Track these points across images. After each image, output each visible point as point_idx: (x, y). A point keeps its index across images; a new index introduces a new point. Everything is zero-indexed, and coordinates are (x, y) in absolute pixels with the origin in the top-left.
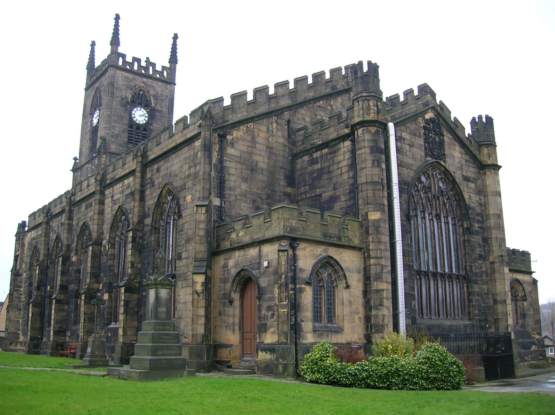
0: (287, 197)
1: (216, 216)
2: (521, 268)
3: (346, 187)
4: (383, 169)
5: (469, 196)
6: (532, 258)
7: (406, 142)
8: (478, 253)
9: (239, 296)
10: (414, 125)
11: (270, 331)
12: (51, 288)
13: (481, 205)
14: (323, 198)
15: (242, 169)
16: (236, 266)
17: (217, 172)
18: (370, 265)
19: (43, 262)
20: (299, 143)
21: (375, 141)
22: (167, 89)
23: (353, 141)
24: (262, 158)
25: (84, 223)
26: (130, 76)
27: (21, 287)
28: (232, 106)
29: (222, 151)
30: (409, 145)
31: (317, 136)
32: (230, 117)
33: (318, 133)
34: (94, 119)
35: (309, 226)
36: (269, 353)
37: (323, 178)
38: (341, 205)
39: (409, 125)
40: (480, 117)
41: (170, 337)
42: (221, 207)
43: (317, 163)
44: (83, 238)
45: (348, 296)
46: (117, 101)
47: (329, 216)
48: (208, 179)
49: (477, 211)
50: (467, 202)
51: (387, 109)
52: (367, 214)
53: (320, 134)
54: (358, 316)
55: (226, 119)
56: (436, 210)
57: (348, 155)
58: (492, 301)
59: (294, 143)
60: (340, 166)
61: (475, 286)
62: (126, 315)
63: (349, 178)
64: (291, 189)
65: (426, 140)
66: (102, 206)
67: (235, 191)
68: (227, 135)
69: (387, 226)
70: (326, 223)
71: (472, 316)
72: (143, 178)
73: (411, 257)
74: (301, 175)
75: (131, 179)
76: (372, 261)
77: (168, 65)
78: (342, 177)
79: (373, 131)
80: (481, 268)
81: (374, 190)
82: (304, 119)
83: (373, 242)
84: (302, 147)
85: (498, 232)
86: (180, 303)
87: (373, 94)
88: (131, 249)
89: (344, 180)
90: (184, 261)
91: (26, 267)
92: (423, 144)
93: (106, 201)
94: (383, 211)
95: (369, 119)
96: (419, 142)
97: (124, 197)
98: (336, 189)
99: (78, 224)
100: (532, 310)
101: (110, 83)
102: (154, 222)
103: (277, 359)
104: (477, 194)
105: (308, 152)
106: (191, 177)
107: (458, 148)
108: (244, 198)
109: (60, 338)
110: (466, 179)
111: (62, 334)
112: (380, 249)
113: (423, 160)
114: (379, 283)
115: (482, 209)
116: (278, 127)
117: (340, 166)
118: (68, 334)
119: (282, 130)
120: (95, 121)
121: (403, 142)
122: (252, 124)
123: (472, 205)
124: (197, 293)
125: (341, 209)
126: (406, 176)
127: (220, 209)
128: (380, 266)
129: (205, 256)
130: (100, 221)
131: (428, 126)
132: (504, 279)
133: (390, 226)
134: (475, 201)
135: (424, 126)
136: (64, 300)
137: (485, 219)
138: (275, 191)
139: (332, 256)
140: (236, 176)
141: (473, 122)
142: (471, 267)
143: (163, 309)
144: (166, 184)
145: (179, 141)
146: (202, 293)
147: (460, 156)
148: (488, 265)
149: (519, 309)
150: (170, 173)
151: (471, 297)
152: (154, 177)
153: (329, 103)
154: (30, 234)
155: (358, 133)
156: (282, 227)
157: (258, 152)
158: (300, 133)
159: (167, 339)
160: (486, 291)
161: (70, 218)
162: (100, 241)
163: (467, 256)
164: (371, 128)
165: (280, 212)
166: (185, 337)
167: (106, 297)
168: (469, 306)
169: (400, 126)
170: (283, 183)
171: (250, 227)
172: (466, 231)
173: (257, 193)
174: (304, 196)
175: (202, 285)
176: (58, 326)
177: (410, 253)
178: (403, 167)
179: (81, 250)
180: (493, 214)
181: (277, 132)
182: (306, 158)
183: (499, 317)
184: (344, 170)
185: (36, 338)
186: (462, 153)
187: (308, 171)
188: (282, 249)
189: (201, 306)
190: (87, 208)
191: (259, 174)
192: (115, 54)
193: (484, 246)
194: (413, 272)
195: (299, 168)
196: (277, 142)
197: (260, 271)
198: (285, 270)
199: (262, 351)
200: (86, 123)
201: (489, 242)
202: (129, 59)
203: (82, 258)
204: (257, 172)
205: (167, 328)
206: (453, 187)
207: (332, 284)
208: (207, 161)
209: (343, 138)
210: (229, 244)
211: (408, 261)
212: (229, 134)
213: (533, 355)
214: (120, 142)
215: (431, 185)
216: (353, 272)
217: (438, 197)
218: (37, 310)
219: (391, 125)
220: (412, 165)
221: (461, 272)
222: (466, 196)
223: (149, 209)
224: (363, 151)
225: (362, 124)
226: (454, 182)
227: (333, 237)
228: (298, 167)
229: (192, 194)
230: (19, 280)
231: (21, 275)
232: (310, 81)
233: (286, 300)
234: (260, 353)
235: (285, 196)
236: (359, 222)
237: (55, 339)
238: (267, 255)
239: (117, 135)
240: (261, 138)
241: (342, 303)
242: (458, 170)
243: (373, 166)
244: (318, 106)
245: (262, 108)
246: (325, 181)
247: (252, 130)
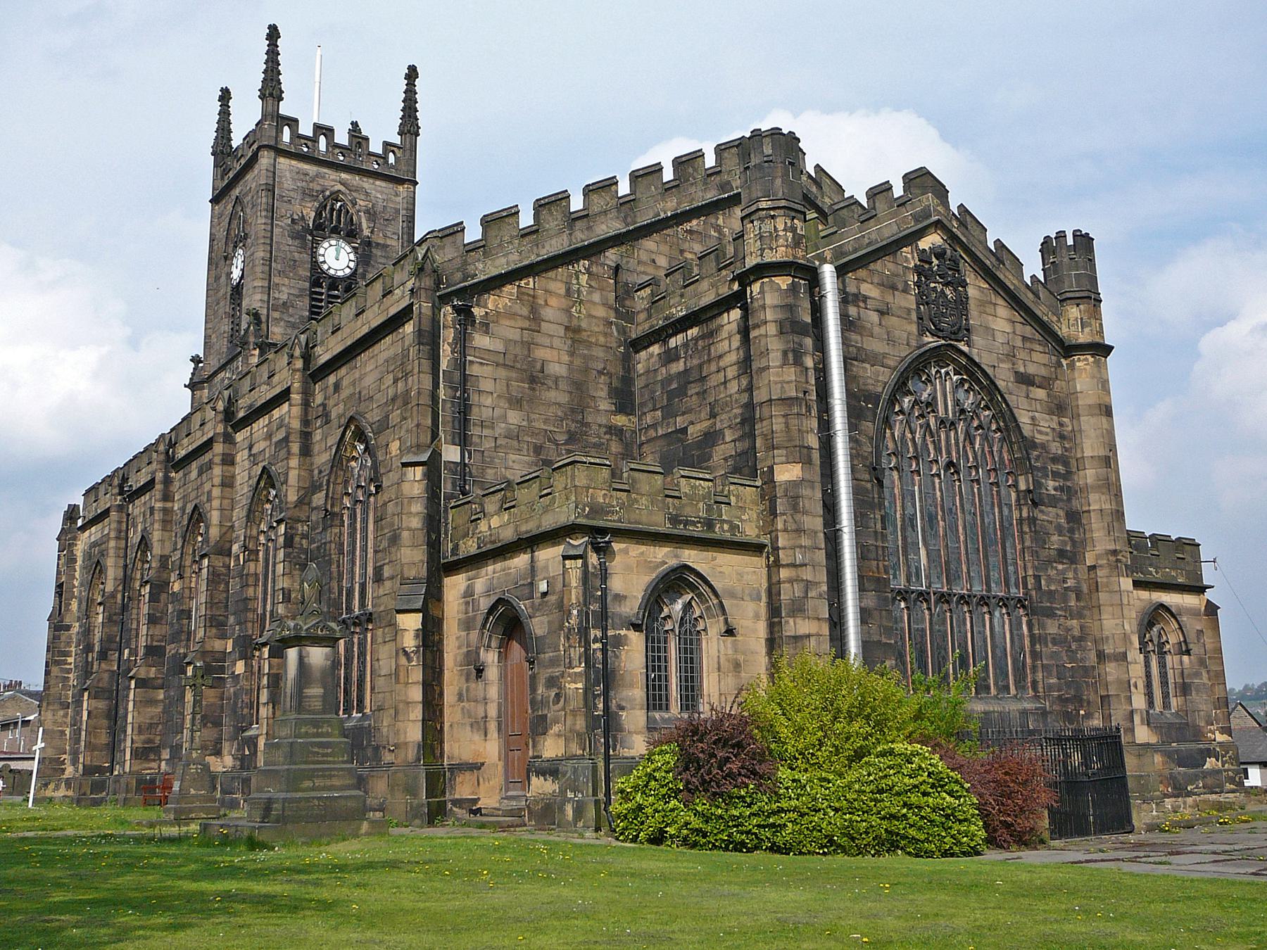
0: (616, 435)
1: (449, 486)
2: (1176, 578)
3: (735, 411)
5: (1033, 418)
6: (1204, 554)
7: (870, 303)
8: (1056, 546)
9: (496, 657)
10: (890, 266)
11: (552, 732)
12: (130, 654)
13: (1062, 437)
14: (689, 437)
15: (508, 380)
16: (488, 593)
17: (451, 388)
18: (779, 582)
19: (113, 595)
20: (642, 316)
21: (790, 308)
22: (397, 195)
23: (745, 309)
24: (555, 353)
25: (196, 506)
26: (311, 169)
27: (68, 654)
28: (483, 243)
29: (462, 342)
30: (878, 311)
31: (678, 299)
32: (480, 266)
33: (679, 292)
34: (234, 268)
35: (636, 501)
36: (550, 779)
37: (689, 393)
38: (723, 451)
39: (877, 266)
41: (330, 750)
42: (463, 464)
43: (677, 358)
44: (195, 539)
45: (730, 652)
46: (281, 227)
47: (683, 477)
48: (429, 406)
49: (1054, 450)
50: (1027, 430)
51: (822, 234)
52: (771, 469)
53: (682, 296)
55: (471, 269)
56: (949, 453)
57: (736, 341)
58: (1093, 656)
59: (629, 316)
60: (722, 364)
61: (1049, 622)
62: (273, 708)
63: (740, 392)
64: (624, 418)
65: (922, 299)
66: (231, 468)
67: (493, 428)
68: (472, 307)
69: (818, 495)
70: (676, 494)
71: (1041, 690)
72: (306, 404)
73: (884, 560)
74: (647, 386)
75: (286, 406)
76: (784, 573)
77: (397, 140)
78: (726, 388)
79: (784, 287)
80: (1064, 581)
81: (785, 416)
82: (654, 261)
83: (785, 530)
84: (647, 326)
86: (379, 676)
87: (783, 203)
88: (284, 561)
89: (730, 396)
90: (388, 584)
91: (79, 608)
92: (914, 307)
93: (238, 458)
94: (807, 461)
95: (774, 259)
96: (904, 304)
97: (273, 447)
98: (715, 417)
99: (183, 509)
100: (1205, 675)
101: (264, 187)
102: (329, 502)
103: (563, 792)
104: (1051, 413)
105: (658, 336)
106: (399, 402)
107: (1003, 311)
108: (515, 443)
109: (147, 766)
110: (1025, 380)
111: (152, 757)
112: (801, 547)
113: (914, 343)
114: (799, 621)
115: (1067, 446)
116: (593, 284)
117: (722, 364)
118: (166, 754)
119: (602, 290)
120: (236, 274)
121: (862, 304)
122: (531, 280)
123: (1040, 438)
124: (406, 653)
125: (725, 459)
126: (870, 381)
127: (461, 468)
128: (802, 585)
129: (424, 573)
130: (226, 502)
131: (927, 266)
132: (1122, 605)
133: (824, 492)
134: (1048, 430)
135: (915, 265)
136: (156, 678)
137: (1074, 470)
138: (588, 425)
139: (691, 564)
140: (495, 395)
141: (1048, 248)
142: (1037, 578)
143: (315, 691)
144: (351, 419)
145: (375, 324)
146: (416, 652)
147: (1008, 329)
148: (1083, 574)
149: (1170, 673)
150: (360, 392)
151: (1038, 646)
152: (331, 402)
153: (713, 221)
154: (87, 533)
155: (751, 292)
156: (572, 506)
157: (547, 341)
158: (643, 293)
159: (324, 755)
160: (1076, 633)
161: (167, 497)
162: (228, 545)
164: (777, 280)
165: (569, 473)
166: (390, 750)
167: (240, 667)
168: (1034, 668)
169: (855, 270)
170: (605, 405)
171: (513, 507)
172: (1025, 498)
173: (546, 430)
174: (652, 433)
175: (417, 636)
176: (142, 737)
177: (880, 552)
178: (863, 362)
179: (191, 566)
181: (589, 293)
182: (655, 349)
184: (732, 372)
185: (100, 770)
187: (659, 378)
188: (572, 553)
189: (415, 680)
190: (200, 474)
191: (549, 388)
192: (274, 119)
193: (1071, 531)
195: (641, 372)
196: (590, 316)
197: (533, 603)
198: (577, 598)
199: (537, 776)
200: (217, 278)
201: (1084, 521)
202: (306, 129)
203: (193, 585)
204: (543, 384)
205: (324, 730)
206: (991, 401)
207: (695, 626)
208: (426, 364)
209: (724, 305)
210: (475, 545)
211: (875, 570)
212: (478, 305)
213: (1209, 781)
214: (291, 319)
215: (935, 398)
217: (952, 424)
218: (101, 705)
219: (828, 271)
220: (885, 355)
221: (1013, 590)
222: (1024, 419)
223: (320, 472)
224: (762, 331)
225: (762, 270)
226: (991, 388)
227: (694, 524)
228: (640, 368)
229: (400, 439)
230: (63, 638)
231: (68, 628)
232: (668, 175)
233: (580, 663)
234: (534, 779)
235: (611, 434)
236: (757, 487)
237: (135, 768)
238: (546, 568)
239: (284, 304)
240: (552, 311)
241: (716, 666)
242: (1003, 361)
243: (785, 363)
244: (686, 231)
245: (553, 242)
246: (694, 398)
247: (531, 292)
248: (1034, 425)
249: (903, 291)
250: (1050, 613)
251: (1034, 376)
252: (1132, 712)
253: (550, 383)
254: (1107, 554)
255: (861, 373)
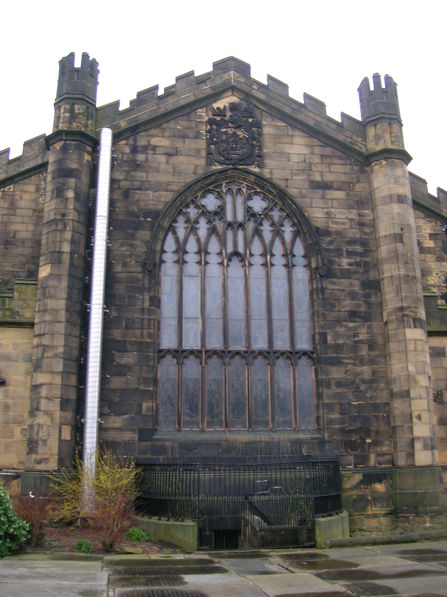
4: (67, 199)
8: (347, 309)
13: (361, 224)
24: (24, 226)
30: (166, 154)
40: (376, 77)
54: (20, 428)
71: (322, 424)
85: (393, 266)
122: (12, 186)
151: (320, 389)
163: (315, 318)
173: (12, 272)
178: (146, 190)
180: (385, 236)
183: (397, 424)
186: (312, 146)
191: (18, 247)
193: (367, 296)
194: (152, 354)
211: (139, 336)
216: (16, 361)
248: (328, 218)
249: (194, 138)
250: (337, 362)
251: (332, 182)
252: (413, 440)
253: (19, 243)
254: (396, 311)
255: (143, 197)
